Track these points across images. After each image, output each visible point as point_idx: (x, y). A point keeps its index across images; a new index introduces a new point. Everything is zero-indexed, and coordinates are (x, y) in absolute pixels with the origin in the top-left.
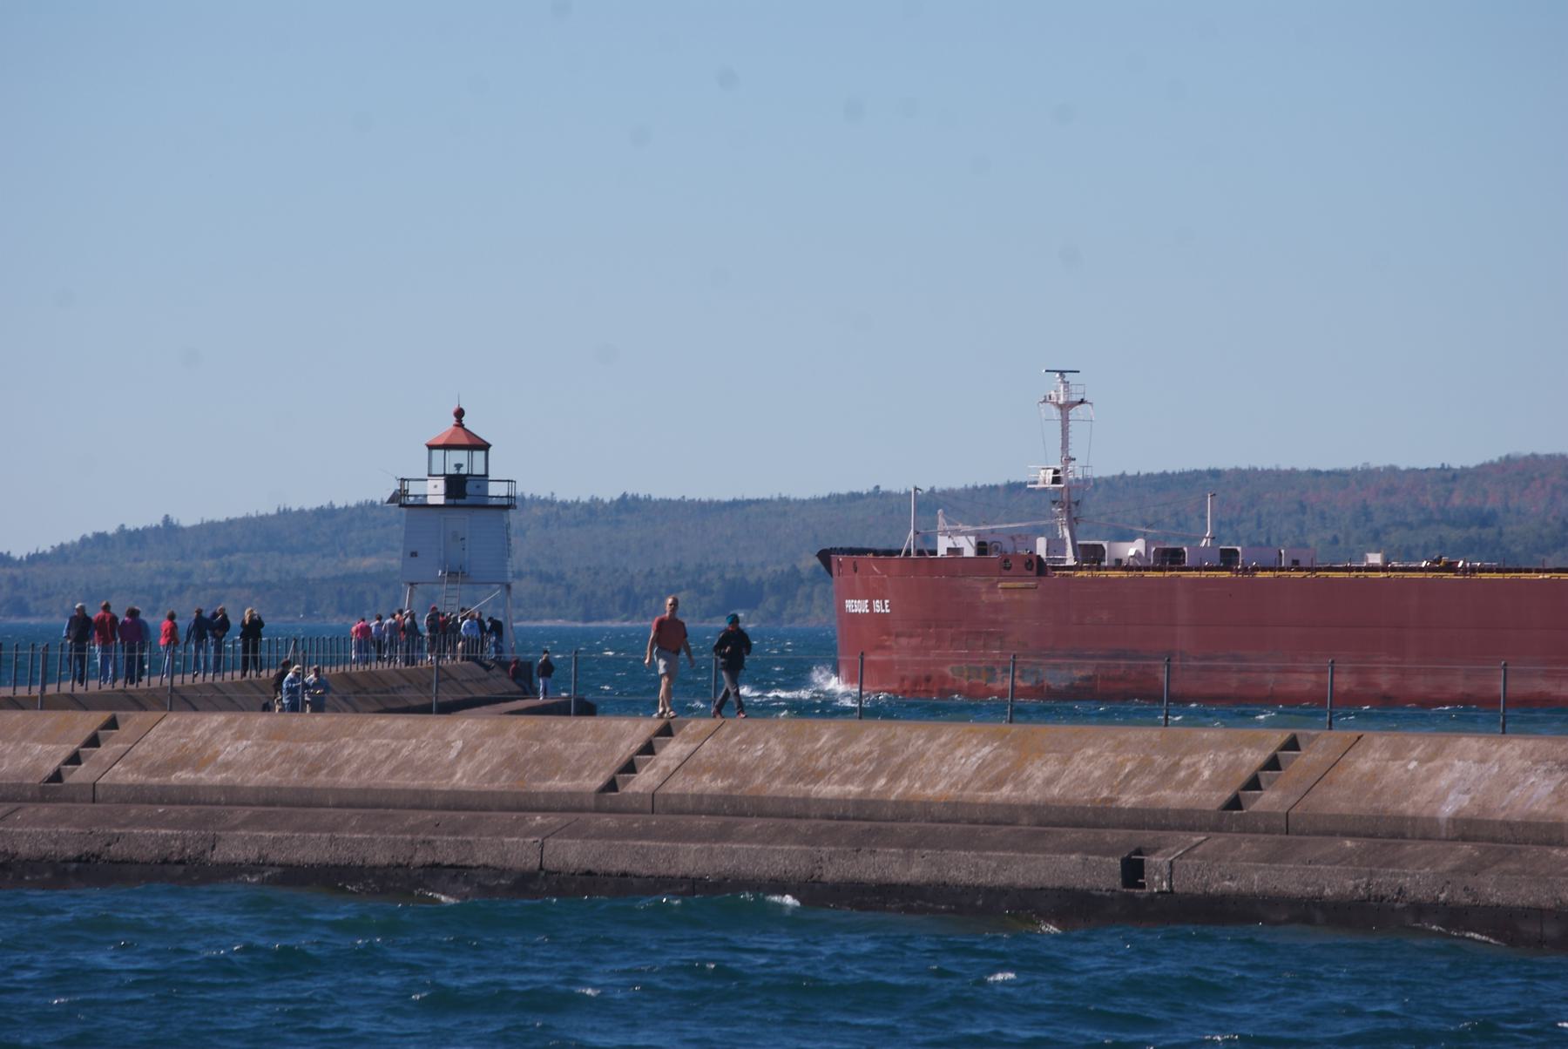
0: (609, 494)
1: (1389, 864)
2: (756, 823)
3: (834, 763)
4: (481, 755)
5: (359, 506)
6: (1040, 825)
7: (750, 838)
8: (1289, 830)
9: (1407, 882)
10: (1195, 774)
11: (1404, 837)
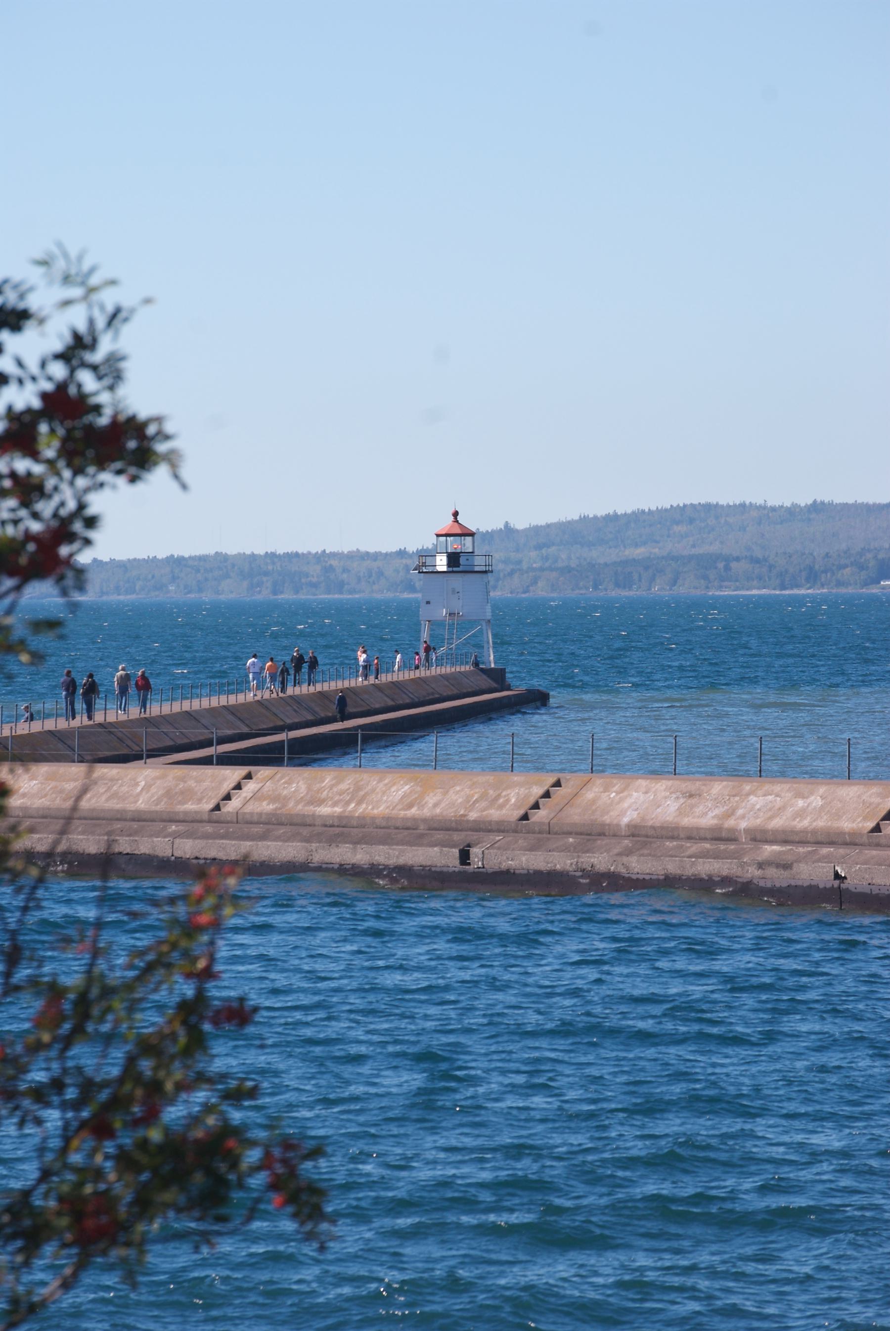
0: (804, 500)
1: (587, 851)
2: (281, 830)
3: (330, 795)
4: (153, 790)
5: (633, 513)
6: (429, 829)
7: (277, 839)
8: (549, 831)
9: (594, 861)
10: (508, 800)
11: (604, 835)
